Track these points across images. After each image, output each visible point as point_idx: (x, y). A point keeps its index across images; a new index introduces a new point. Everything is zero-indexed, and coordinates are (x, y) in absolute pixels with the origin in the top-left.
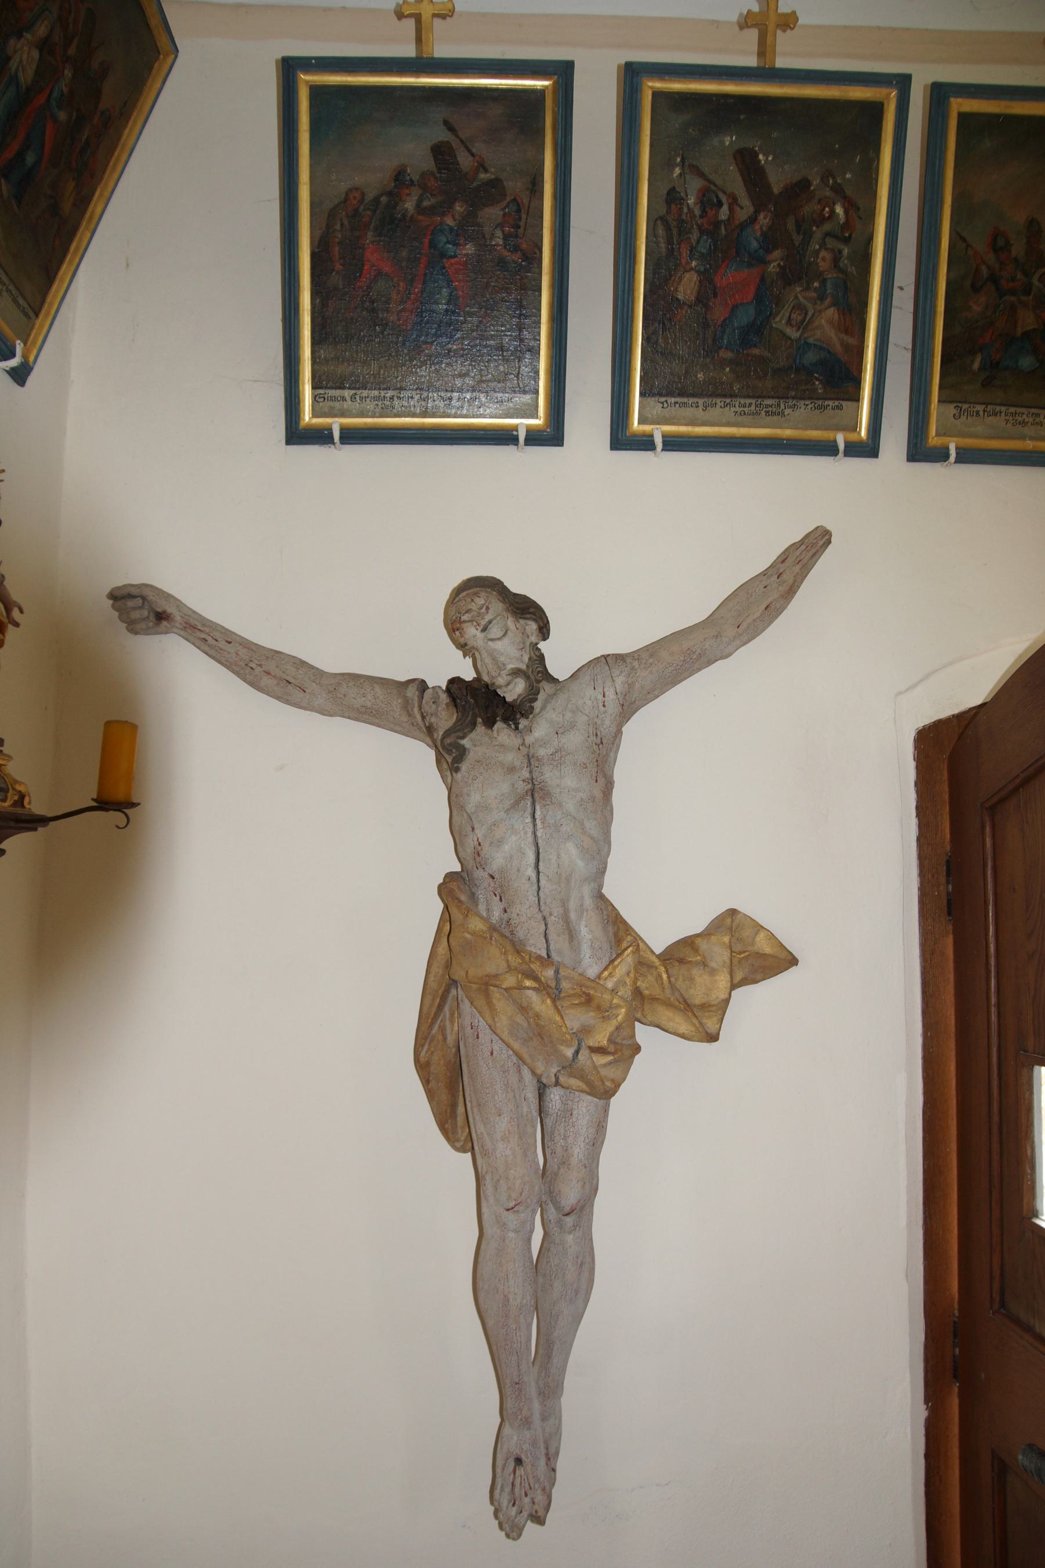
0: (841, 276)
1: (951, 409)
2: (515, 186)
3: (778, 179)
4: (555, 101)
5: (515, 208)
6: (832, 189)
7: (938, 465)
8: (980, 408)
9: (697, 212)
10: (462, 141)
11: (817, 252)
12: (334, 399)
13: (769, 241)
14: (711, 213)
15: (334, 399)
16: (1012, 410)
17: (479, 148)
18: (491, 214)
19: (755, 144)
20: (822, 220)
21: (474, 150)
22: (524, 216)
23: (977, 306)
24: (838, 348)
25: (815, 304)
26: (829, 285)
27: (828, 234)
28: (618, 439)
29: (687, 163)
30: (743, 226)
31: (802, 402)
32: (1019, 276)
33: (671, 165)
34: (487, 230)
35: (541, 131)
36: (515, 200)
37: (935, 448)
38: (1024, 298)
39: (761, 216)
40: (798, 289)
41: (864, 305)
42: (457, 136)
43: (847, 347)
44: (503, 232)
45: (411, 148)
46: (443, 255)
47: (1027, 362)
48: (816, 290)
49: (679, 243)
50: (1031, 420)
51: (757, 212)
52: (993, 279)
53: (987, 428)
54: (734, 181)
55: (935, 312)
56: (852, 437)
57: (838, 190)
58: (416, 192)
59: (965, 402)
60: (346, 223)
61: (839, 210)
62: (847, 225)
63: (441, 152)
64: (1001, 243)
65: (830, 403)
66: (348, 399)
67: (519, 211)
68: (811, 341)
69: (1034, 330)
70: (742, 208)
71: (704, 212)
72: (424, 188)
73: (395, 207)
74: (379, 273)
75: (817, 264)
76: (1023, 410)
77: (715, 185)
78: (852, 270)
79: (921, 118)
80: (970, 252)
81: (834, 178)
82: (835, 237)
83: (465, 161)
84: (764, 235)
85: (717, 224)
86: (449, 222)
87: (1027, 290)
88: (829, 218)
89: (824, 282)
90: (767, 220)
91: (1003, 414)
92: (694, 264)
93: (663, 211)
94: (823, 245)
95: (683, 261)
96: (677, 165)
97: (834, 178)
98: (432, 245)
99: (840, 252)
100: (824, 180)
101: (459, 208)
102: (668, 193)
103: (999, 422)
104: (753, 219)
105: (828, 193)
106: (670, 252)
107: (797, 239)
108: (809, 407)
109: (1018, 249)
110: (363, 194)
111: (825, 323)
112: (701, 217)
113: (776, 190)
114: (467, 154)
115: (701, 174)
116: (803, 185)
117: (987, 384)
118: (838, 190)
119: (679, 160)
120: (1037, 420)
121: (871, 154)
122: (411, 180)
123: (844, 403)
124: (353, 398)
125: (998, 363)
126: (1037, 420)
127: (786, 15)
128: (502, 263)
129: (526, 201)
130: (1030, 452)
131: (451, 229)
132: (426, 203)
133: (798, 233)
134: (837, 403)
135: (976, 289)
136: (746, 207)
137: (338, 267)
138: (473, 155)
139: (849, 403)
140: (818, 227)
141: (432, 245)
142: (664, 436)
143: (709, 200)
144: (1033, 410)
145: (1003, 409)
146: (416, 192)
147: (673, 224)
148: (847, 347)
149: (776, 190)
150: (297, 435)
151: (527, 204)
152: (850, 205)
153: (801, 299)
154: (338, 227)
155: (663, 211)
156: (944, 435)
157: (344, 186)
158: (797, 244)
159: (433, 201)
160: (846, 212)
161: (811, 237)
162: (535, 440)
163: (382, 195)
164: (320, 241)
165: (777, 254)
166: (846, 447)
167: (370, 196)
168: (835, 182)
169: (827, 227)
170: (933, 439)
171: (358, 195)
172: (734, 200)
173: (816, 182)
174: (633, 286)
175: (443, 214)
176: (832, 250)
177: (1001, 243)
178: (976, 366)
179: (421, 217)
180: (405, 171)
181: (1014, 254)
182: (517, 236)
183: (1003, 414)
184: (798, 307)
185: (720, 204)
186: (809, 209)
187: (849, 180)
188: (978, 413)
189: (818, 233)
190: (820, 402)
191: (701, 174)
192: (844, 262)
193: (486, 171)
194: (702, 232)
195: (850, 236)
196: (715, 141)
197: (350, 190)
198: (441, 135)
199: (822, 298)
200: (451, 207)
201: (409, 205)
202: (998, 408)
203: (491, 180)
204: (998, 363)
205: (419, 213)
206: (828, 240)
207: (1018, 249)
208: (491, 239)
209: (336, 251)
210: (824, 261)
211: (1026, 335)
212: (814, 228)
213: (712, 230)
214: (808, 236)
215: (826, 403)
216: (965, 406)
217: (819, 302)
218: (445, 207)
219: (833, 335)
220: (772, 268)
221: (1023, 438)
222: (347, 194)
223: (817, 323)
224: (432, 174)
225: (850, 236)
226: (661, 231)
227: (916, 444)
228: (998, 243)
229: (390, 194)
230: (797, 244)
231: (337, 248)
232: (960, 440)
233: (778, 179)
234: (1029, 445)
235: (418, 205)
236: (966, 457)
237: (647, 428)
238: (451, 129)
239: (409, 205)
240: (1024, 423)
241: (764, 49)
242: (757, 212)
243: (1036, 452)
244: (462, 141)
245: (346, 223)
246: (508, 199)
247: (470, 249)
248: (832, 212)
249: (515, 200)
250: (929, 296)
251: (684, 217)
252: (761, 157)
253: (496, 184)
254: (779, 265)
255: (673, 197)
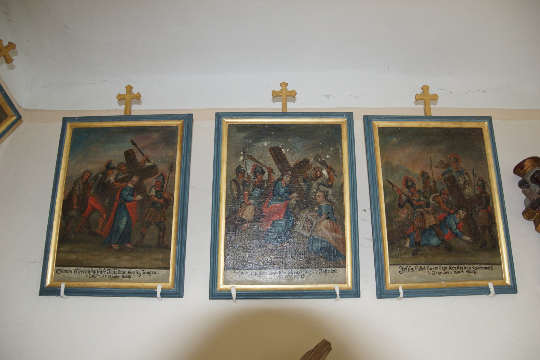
0: (329, 203)
1: (397, 268)
2: (162, 168)
3: (292, 159)
4: (183, 130)
5: (162, 178)
6: (320, 163)
7: (395, 299)
8: (413, 267)
9: (252, 177)
10: (139, 149)
11: (316, 193)
12: (65, 272)
13: (290, 189)
14: (259, 177)
15: (65, 272)
16: (431, 266)
17: (147, 152)
18: (151, 181)
19: (281, 145)
20: (316, 178)
21: (144, 153)
22: (166, 182)
23: (403, 214)
24: (332, 241)
25: (317, 218)
26: (323, 209)
27: (320, 184)
28: (212, 293)
29: (246, 154)
30: (276, 183)
31: (314, 269)
32: (422, 199)
33: (237, 155)
34: (148, 189)
35: (176, 144)
36: (162, 174)
37: (391, 290)
38: (427, 209)
39: (285, 177)
40: (307, 211)
41: (343, 218)
42: (137, 147)
43: (336, 239)
44: (155, 189)
45: (116, 154)
46: (126, 201)
47: (434, 241)
48: (316, 211)
49: (243, 191)
50: (442, 271)
51: (283, 175)
52: (409, 201)
53: (420, 277)
54: (271, 162)
55: (381, 219)
56: (344, 286)
57: (323, 163)
58: (115, 172)
59: (405, 264)
60: (81, 187)
61: (325, 172)
62: (328, 180)
63: (129, 154)
64: (410, 184)
65: (330, 269)
66: (73, 272)
67: (164, 179)
68: (316, 237)
69: (435, 224)
70: (275, 174)
71: (255, 176)
72: (119, 170)
73: (105, 179)
74: (94, 209)
75: (316, 199)
76: (437, 266)
77: (261, 164)
78: (335, 200)
79: (18, 129)
80: (395, 189)
81: (320, 158)
82: (324, 185)
83: (139, 158)
84: (288, 186)
85: (262, 182)
86: (130, 185)
87: (428, 205)
88: (320, 176)
89: (320, 207)
90: (288, 179)
91: (426, 269)
92: (251, 201)
93: (234, 177)
94: (318, 189)
95: (246, 200)
96: (242, 156)
97: (320, 158)
98: (121, 196)
99: (327, 192)
100: (316, 159)
101: (135, 179)
102: (238, 168)
103: (425, 273)
104: (281, 179)
105: (318, 165)
106: (239, 195)
107: (305, 188)
108: (319, 272)
109: (419, 186)
110: (91, 173)
111: (324, 229)
112: (254, 179)
113: (292, 165)
114: (141, 155)
115: (254, 160)
116: (306, 161)
117: (414, 254)
118: (323, 163)
119: (242, 153)
120: (446, 271)
121: (338, 147)
122: (114, 167)
123: (337, 269)
124: (75, 271)
125: (419, 243)
126: (446, 271)
127: (290, 92)
128: (154, 204)
129: (167, 175)
130: (445, 288)
131: (130, 188)
132: (120, 177)
133: (305, 183)
134: (333, 269)
135: (401, 206)
136: (277, 174)
137: (75, 207)
138: (143, 155)
139: (341, 269)
140: (314, 181)
141: (121, 196)
142: (237, 290)
143: (258, 171)
144: (442, 266)
145: (426, 266)
146: (115, 172)
147: (240, 182)
148: (336, 239)
149: (292, 165)
150: (489, 119)
151: (168, 176)
152: (330, 170)
153: (309, 216)
154: (77, 188)
155: (234, 177)
156: (396, 282)
157: (83, 171)
158: (305, 189)
159: (123, 176)
160: (328, 173)
161: (311, 186)
162: (166, 294)
163: (100, 174)
164: (69, 194)
165: (294, 195)
166: (340, 292)
167: (94, 174)
168: (322, 160)
169: (319, 181)
170: (390, 284)
171: (88, 174)
172: (270, 170)
173: (312, 160)
174: (219, 213)
175: (127, 182)
176: (323, 192)
177: (410, 184)
178: (407, 245)
179: (116, 183)
180: (111, 163)
181: (417, 189)
182: (162, 191)
183: (426, 269)
184: (308, 220)
185: (264, 172)
186: (310, 172)
187: (328, 159)
188: (412, 269)
189: (315, 184)
190: (324, 269)
191: (254, 160)
192: (330, 197)
193: (149, 162)
194: (255, 186)
195: (332, 184)
196: (260, 144)
197: (85, 172)
198: (131, 147)
199: (320, 215)
200: (131, 178)
201: (112, 178)
202: (423, 266)
203: (152, 166)
204: (419, 243)
205: (116, 182)
206: (321, 187)
207: (419, 186)
208: (150, 192)
209: (75, 200)
210: (319, 197)
211: (431, 227)
212: (313, 182)
213: (260, 185)
214: (310, 187)
215: (328, 269)
216: (405, 266)
217: (319, 217)
218: (128, 179)
219: (328, 234)
220: (293, 202)
221: (439, 281)
222: (84, 173)
223: (319, 228)
224: (124, 164)
225: (332, 184)
226: (234, 187)
227: (380, 289)
228: (408, 183)
229: (103, 173)
230: (305, 189)
231: (76, 198)
232: (405, 285)
233: (292, 159)
234: (444, 284)
235: (116, 178)
236: (409, 293)
237: (228, 287)
238: (134, 144)
239: (112, 178)
240: (439, 273)
241: (284, 106)
242: (283, 175)
243: (447, 288)
244: (139, 149)
245: (81, 187)
246: (159, 174)
247: (139, 197)
248: (321, 173)
249: (162, 174)
250: (377, 211)
251: (245, 179)
252: (283, 150)
253: (154, 167)
254: (296, 200)
255: (239, 171)
